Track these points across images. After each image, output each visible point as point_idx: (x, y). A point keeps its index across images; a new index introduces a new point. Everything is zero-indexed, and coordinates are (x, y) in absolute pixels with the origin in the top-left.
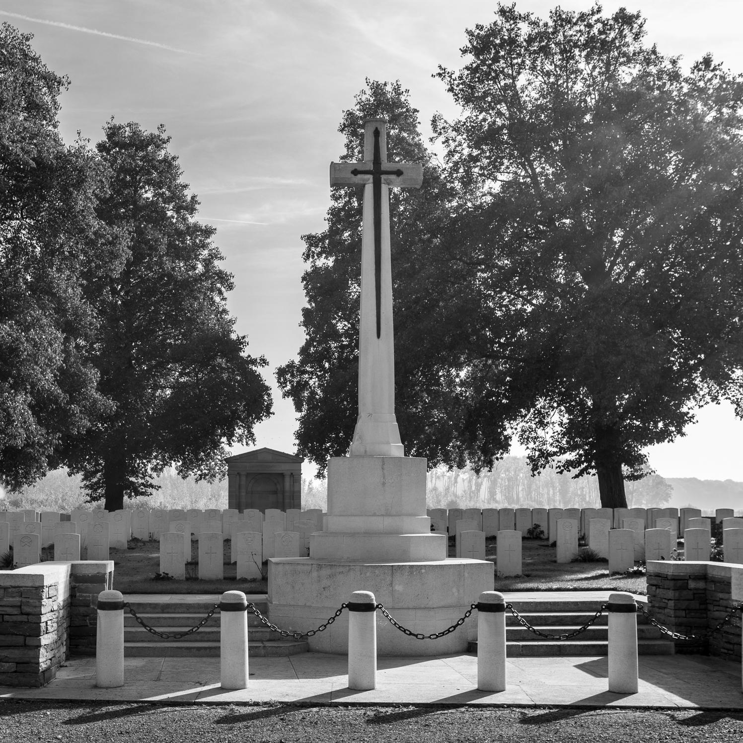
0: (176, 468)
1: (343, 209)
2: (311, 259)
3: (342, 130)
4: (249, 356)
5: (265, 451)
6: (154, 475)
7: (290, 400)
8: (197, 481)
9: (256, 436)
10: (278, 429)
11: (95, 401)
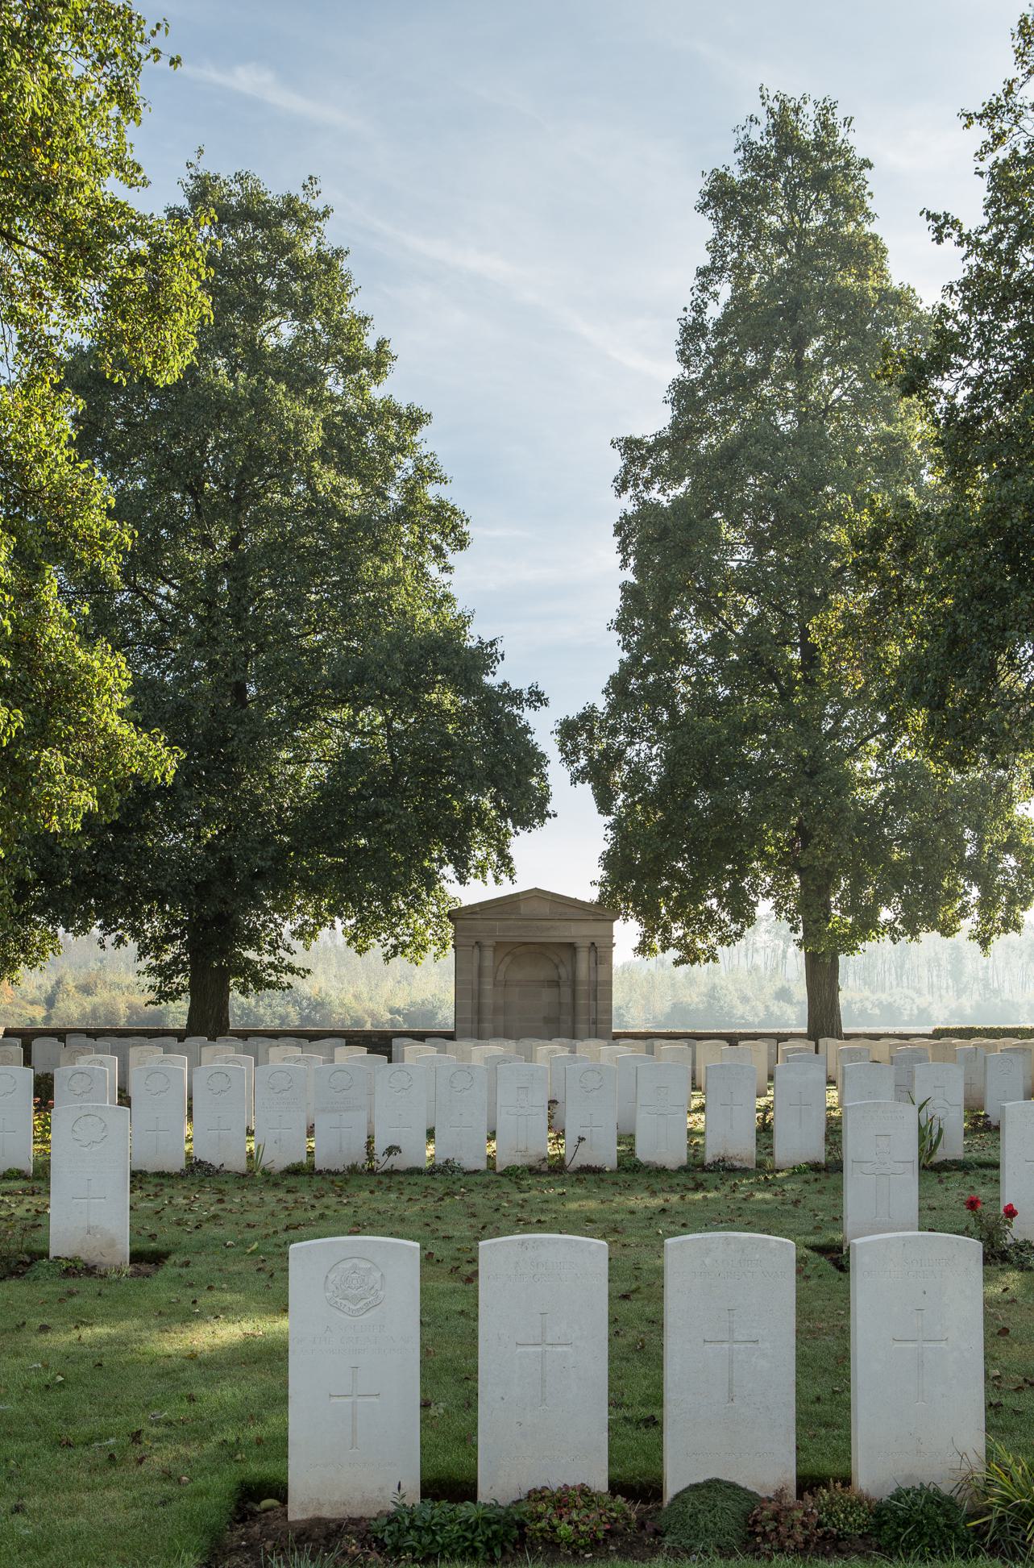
0: (344, 933)
1: (701, 383)
2: (630, 491)
3: (703, 208)
4: (505, 684)
5: (537, 894)
6: (297, 945)
7: (586, 789)
8: (387, 959)
9: (516, 864)
10: (564, 850)
11: (113, 745)
